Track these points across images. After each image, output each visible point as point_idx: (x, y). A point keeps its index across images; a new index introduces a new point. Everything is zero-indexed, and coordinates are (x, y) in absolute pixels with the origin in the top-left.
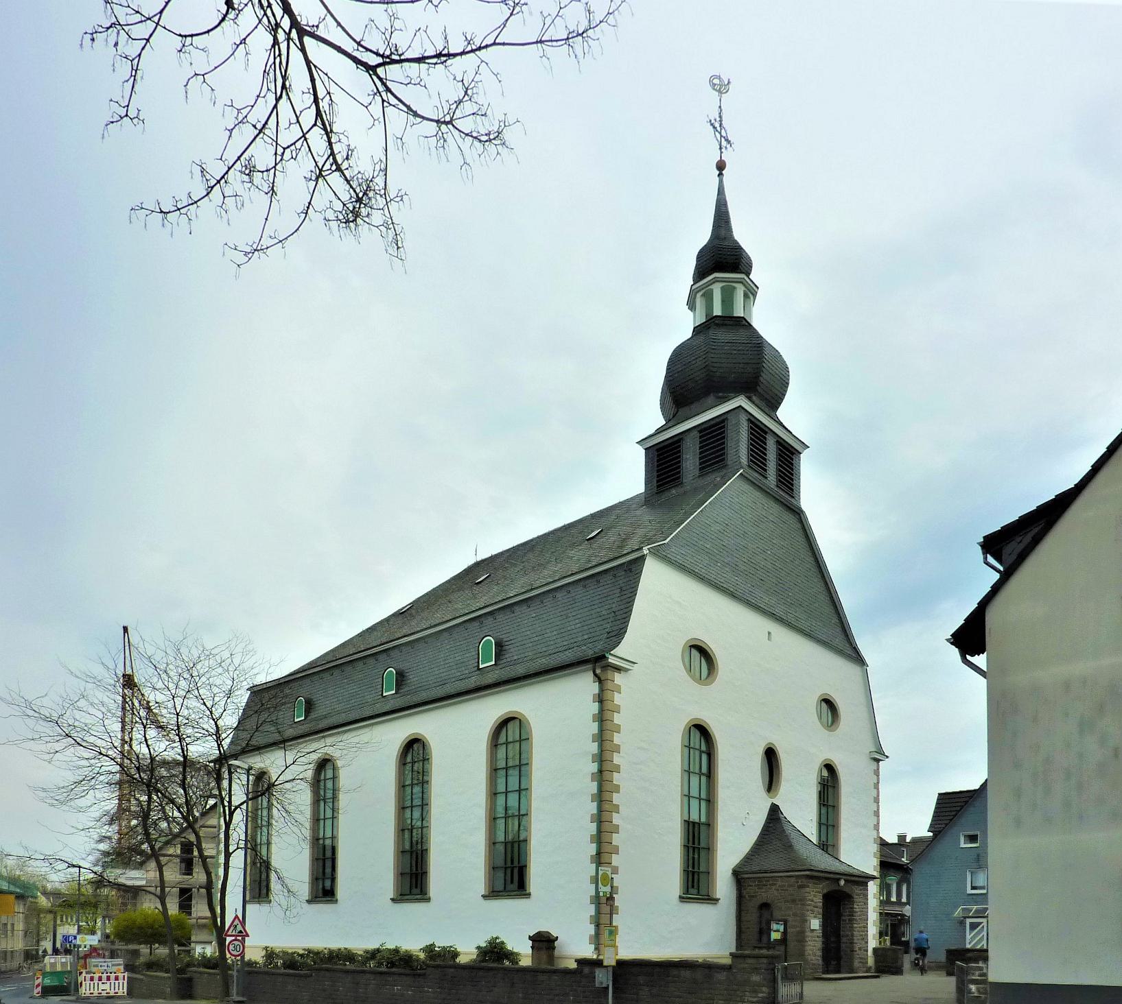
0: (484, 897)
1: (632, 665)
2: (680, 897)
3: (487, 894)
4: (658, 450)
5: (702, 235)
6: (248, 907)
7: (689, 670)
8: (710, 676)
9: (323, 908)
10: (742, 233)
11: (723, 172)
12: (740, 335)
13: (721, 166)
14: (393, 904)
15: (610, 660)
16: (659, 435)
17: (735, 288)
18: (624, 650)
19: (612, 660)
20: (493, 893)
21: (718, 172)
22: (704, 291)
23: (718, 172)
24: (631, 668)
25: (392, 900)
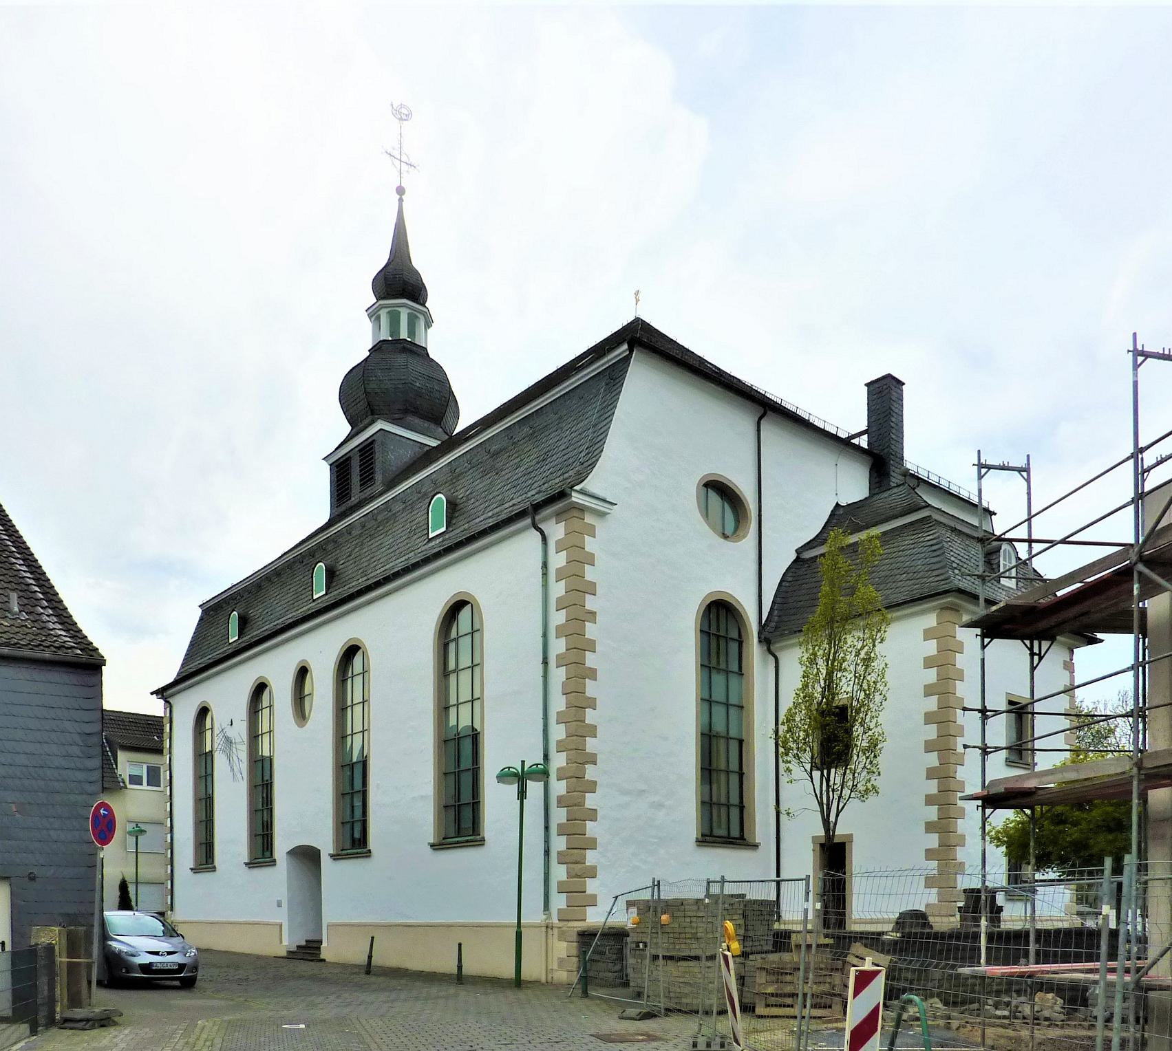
0: (434, 846)
1: (610, 507)
2: (697, 841)
3: (436, 842)
4: (337, 467)
5: (380, 259)
6: (456, 724)
7: (706, 513)
8: (740, 528)
9: (205, 877)
10: (420, 260)
11: (403, 197)
12: (415, 365)
13: (400, 191)
14: (433, 852)
15: (573, 499)
16: (345, 446)
17: (417, 317)
18: (595, 482)
19: (576, 498)
20: (251, 864)
21: (399, 197)
22: (390, 309)
23: (399, 197)
24: (609, 511)
25: (432, 845)
